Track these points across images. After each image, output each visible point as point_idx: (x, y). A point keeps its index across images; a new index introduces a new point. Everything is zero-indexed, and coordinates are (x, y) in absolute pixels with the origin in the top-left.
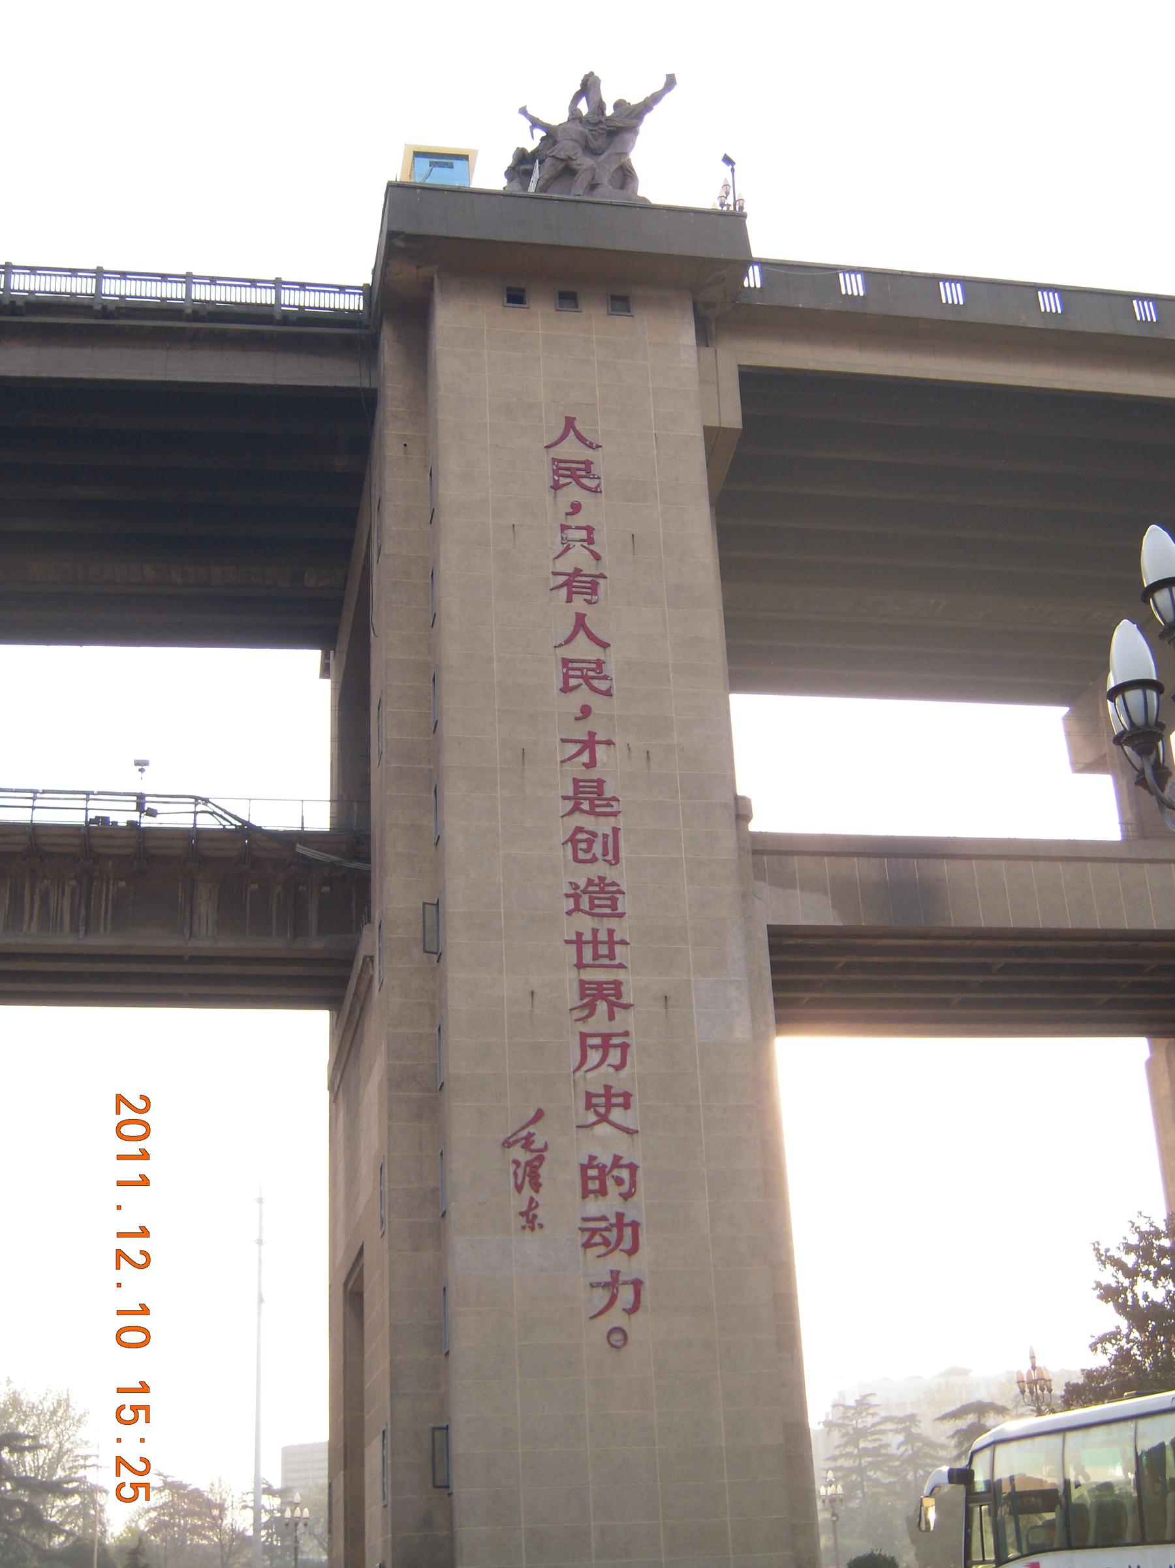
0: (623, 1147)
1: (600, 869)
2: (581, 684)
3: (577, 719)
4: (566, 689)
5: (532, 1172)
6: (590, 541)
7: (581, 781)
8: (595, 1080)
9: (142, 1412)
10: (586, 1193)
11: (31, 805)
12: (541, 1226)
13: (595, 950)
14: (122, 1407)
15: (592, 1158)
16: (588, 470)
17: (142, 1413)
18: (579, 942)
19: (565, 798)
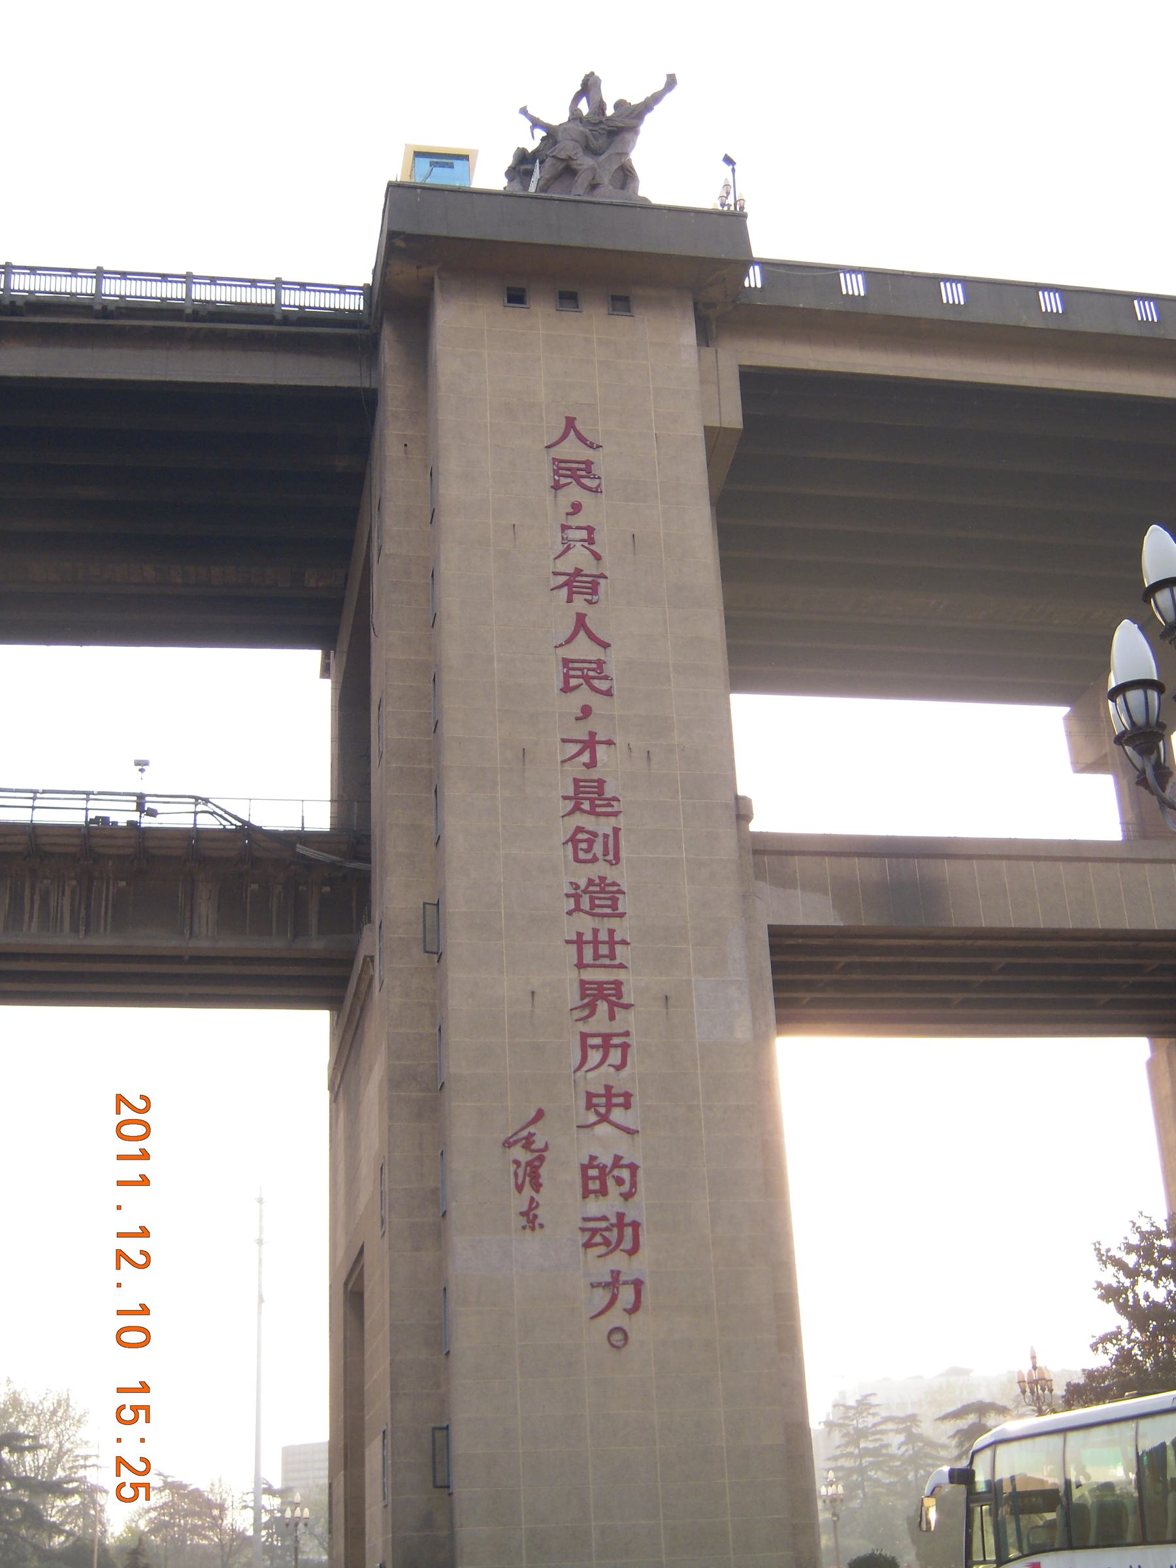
0: (624, 1147)
1: (601, 869)
2: (582, 684)
3: (577, 719)
4: (567, 689)
5: (532, 1172)
6: (591, 541)
7: (582, 781)
8: (595, 1080)
9: (142, 1412)
10: (586, 1193)
11: (31, 805)
12: (541, 1226)
13: (596, 950)
14: (122, 1407)
15: (593, 1158)
16: (588, 470)
17: (142, 1413)
18: (579, 942)
19: (565, 798)
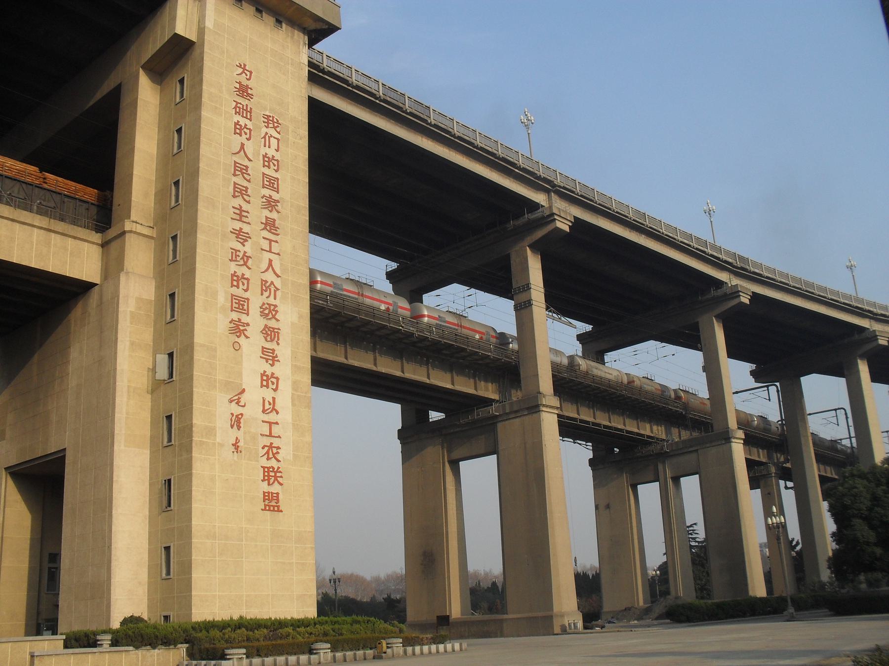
3: (262, 510)
5: (237, 420)
10: (262, 386)
11: (852, 436)
12: (241, 452)
15: (265, 372)
16: (246, 191)
19: (262, 223)
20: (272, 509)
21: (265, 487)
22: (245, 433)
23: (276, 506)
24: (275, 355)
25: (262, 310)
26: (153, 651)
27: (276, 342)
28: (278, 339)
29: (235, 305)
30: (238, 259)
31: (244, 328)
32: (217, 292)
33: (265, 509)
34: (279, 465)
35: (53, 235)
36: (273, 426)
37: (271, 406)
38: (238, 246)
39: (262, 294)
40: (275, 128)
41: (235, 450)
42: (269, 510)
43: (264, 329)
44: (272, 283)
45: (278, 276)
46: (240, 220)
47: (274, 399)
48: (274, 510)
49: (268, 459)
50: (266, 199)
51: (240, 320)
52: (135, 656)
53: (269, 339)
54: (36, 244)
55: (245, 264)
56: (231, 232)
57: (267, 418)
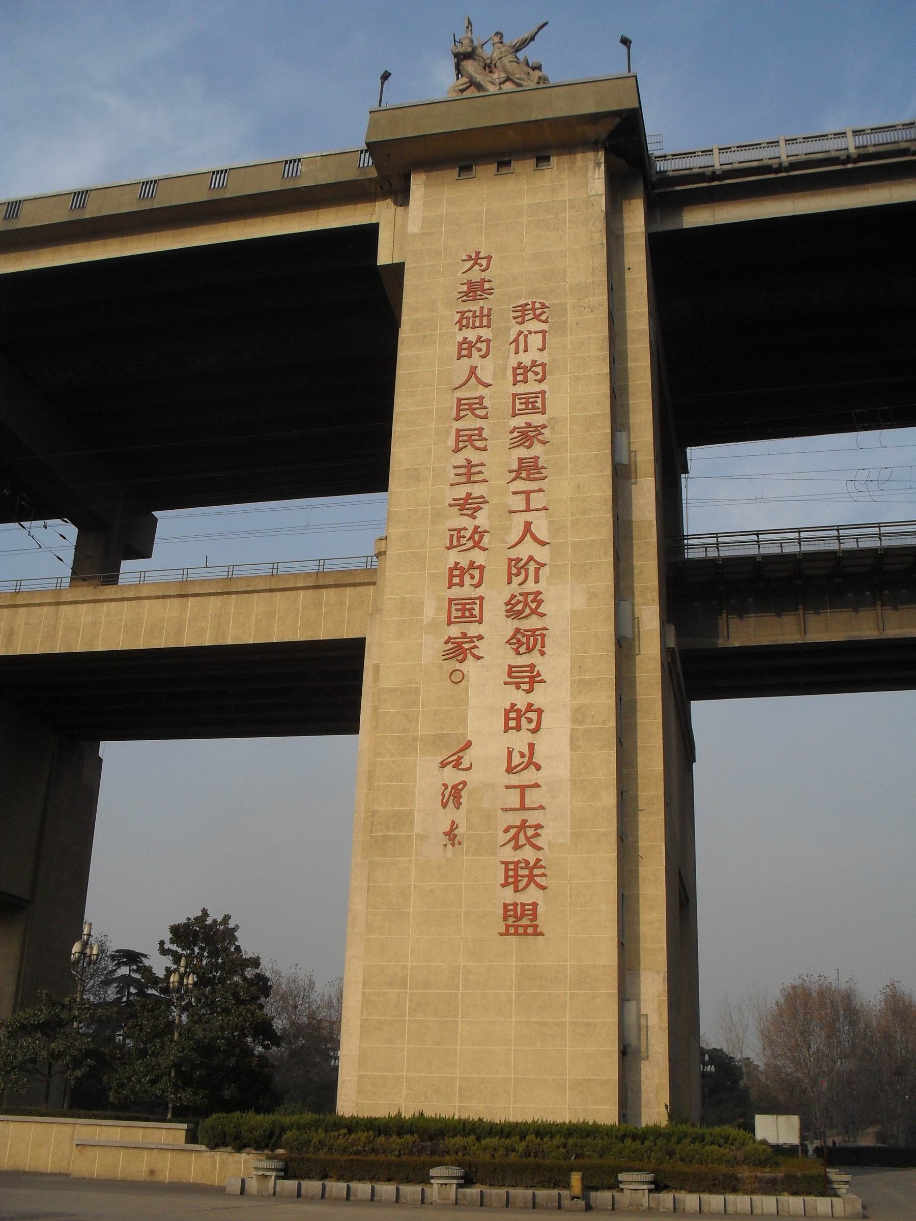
3: (501, 934)
10: (507, 729)
12: (460, 843)
15: (513, 705)
20: (521, 930)
21: (508, 894)
22: (469, 811)
23: (530, 926)
24: (535, 674)
25: (509, 607)
26: (238, 1155)
27: (537, 651)
28: (543, 646)
29: (454, 614)
30: (463, 541)
31: (473, 644)
32: (423, 603)
33: (507, 933)
34: (540, 855)
35: (325, 591)
36: (529, 793)
37: (526, 760)
38: (468, 523)
39: (510, 582)
40: (537, 317)
41: (449, 843)
42: (516, 933)
43: (513, 637)
44: (531, 558)
45: (543, 544)
46: (469, 482)
47: (531, 746)
48: (525, 933)
49: (517, 847)
50: (518, 432)
51: (464, 635)
52: (209, 1160)
53: (522, 649)
54: (302, 611)
55: (477, 545)
56: (451, 505)
57: (514, 780)
